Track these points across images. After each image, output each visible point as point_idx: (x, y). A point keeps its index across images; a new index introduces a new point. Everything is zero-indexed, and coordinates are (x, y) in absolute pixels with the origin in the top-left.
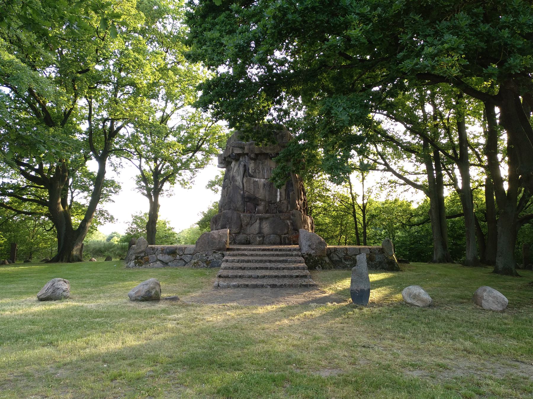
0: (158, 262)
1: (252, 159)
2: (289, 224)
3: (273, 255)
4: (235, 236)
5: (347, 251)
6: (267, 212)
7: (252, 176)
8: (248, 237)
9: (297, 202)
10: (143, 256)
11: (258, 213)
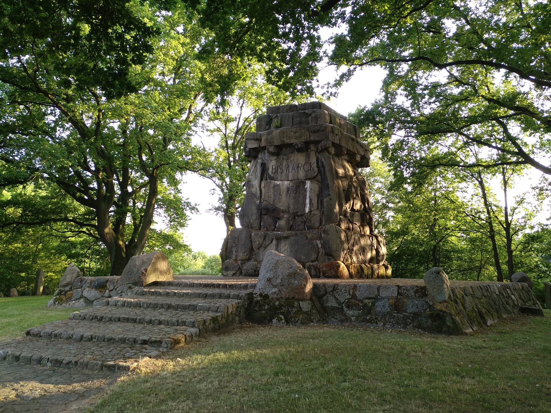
1: (273, 154)
2: (320, 246)
4: (242, 264)
6: (291, 228)
7: (272, 179)
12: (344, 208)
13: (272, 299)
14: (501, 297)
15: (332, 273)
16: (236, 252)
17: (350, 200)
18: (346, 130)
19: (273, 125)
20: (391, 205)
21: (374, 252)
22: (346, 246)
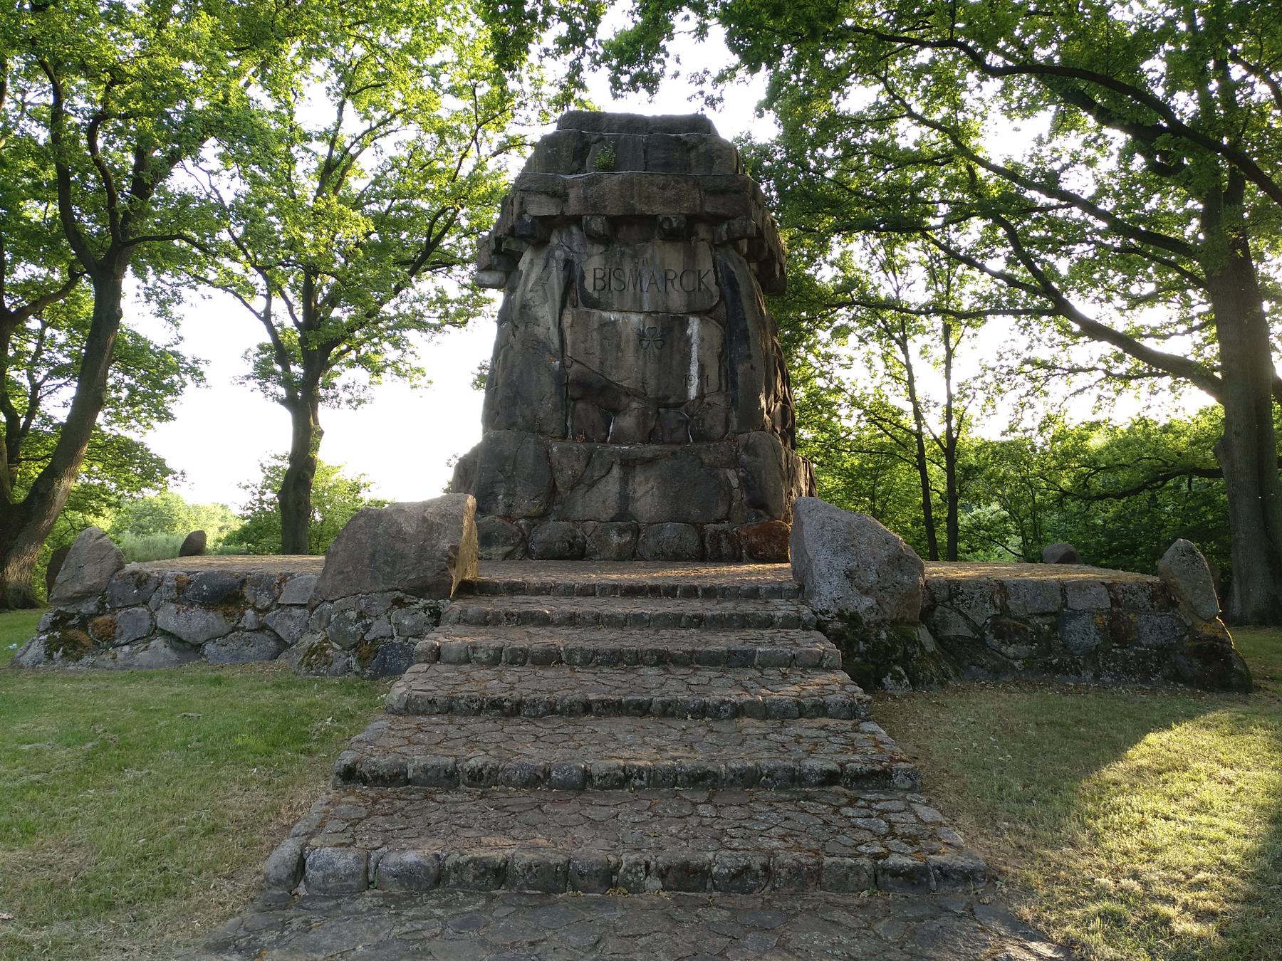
0: (158, 643)
1: (593, 238)
3: (676, 621)
4: (530, 527)
5: (1007, 596)
6: (650, 438)
7: (596, 304)
8: (579, 532)
9: (763, 403)
10: (92, 616)
11: (617, 440)
13: (868, 623)
15: (772, 549)
16: (506, 495)
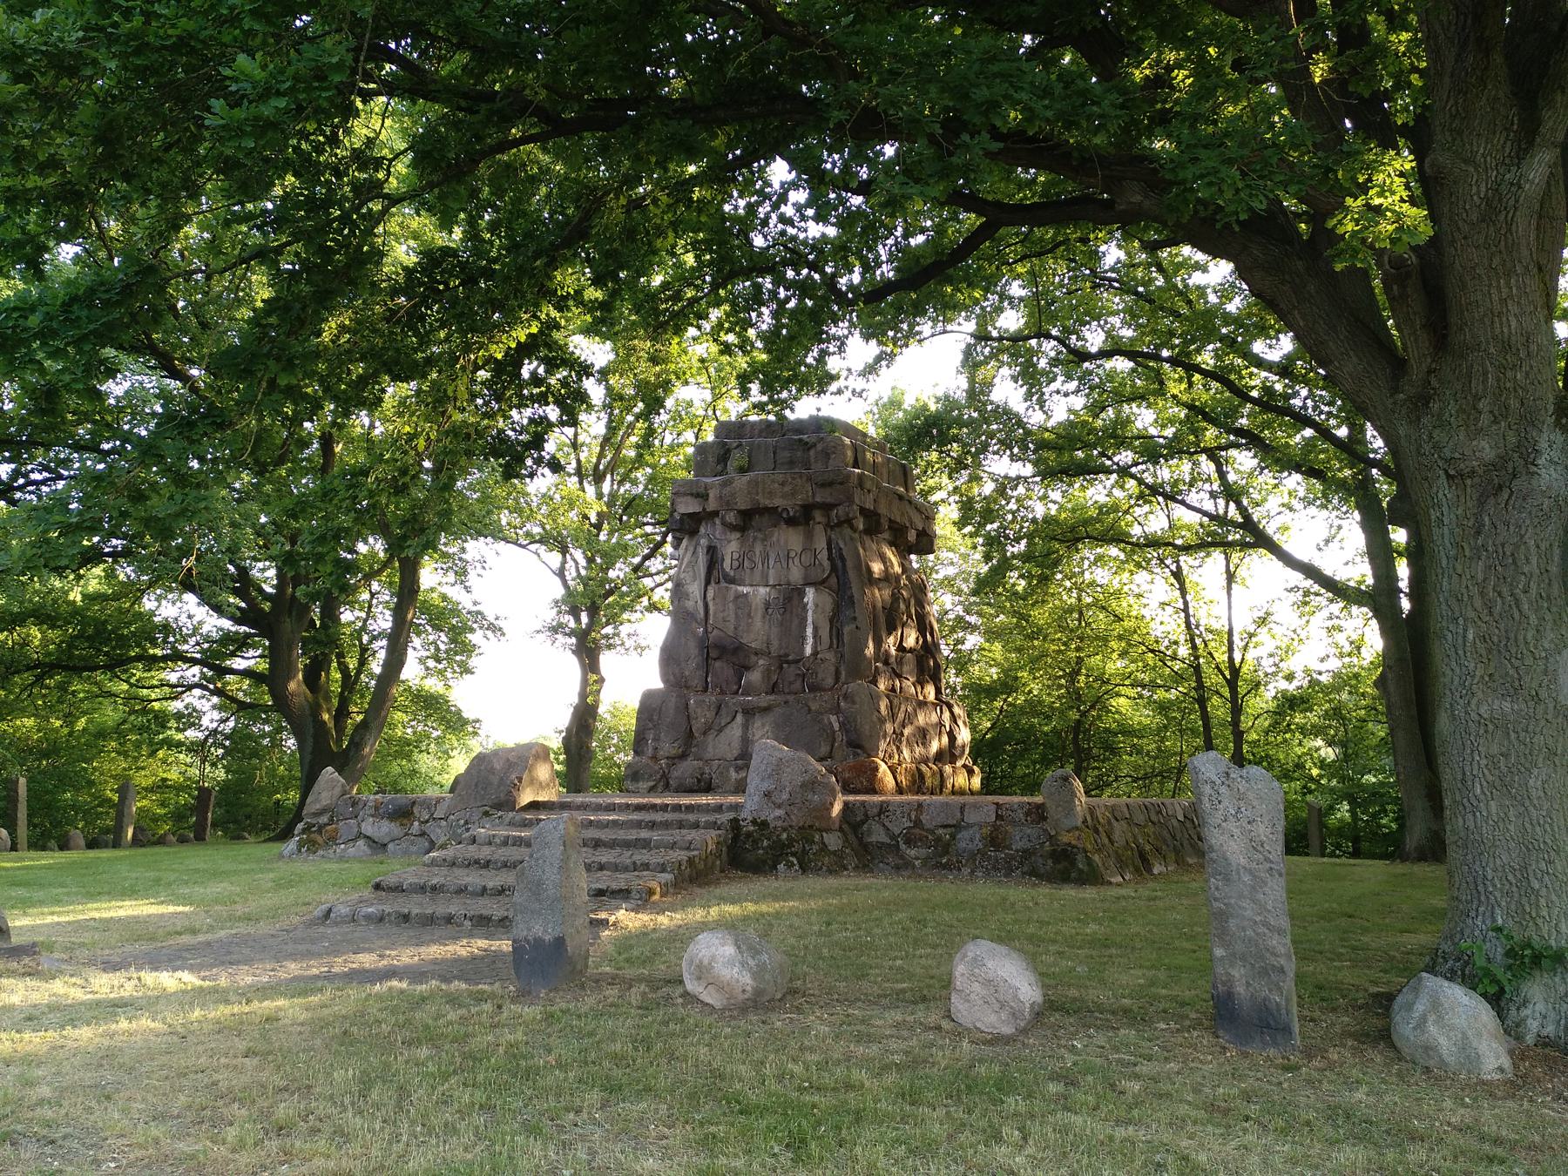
1: (733, 528)
2: (836, 726)
4: (669, 766)
6: (773, 689)
7: (732, 581)
12: (885, 646)
14: (1188, 824)
17: (895, 629)
18: (885, 476)
19: (733, 464)
20: (973, 619)
21: (945, 739)
22: (889, 727)
